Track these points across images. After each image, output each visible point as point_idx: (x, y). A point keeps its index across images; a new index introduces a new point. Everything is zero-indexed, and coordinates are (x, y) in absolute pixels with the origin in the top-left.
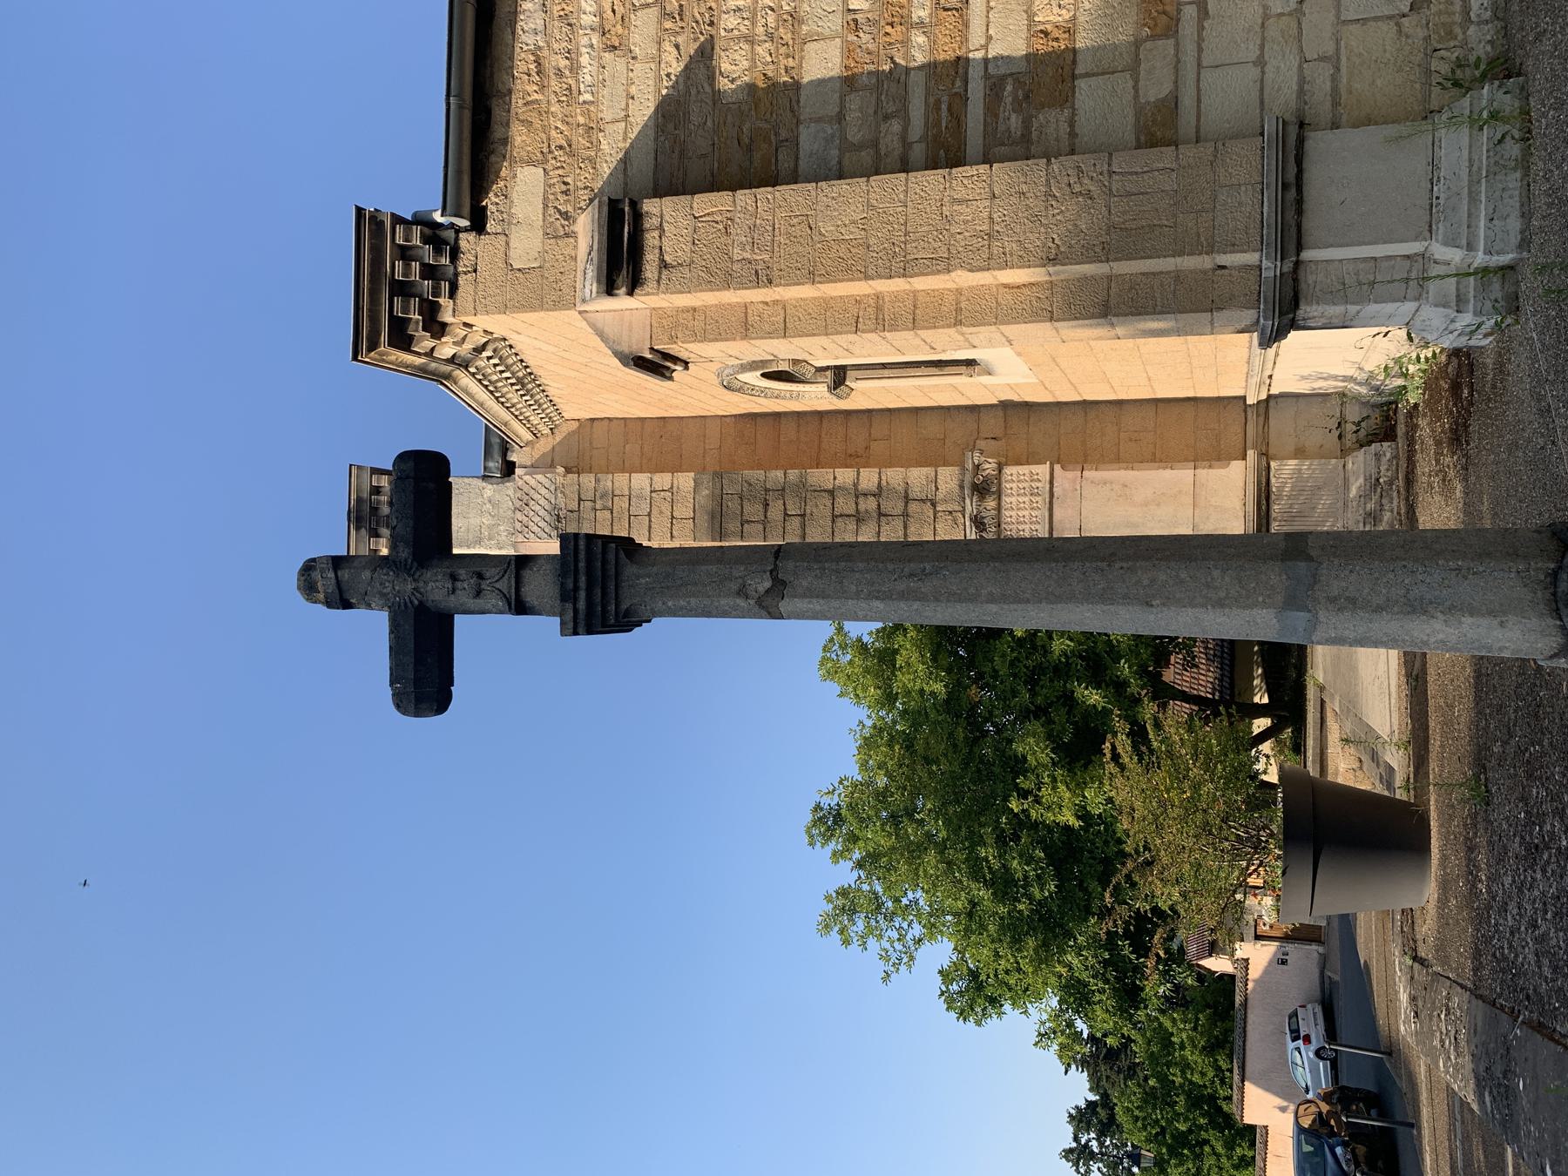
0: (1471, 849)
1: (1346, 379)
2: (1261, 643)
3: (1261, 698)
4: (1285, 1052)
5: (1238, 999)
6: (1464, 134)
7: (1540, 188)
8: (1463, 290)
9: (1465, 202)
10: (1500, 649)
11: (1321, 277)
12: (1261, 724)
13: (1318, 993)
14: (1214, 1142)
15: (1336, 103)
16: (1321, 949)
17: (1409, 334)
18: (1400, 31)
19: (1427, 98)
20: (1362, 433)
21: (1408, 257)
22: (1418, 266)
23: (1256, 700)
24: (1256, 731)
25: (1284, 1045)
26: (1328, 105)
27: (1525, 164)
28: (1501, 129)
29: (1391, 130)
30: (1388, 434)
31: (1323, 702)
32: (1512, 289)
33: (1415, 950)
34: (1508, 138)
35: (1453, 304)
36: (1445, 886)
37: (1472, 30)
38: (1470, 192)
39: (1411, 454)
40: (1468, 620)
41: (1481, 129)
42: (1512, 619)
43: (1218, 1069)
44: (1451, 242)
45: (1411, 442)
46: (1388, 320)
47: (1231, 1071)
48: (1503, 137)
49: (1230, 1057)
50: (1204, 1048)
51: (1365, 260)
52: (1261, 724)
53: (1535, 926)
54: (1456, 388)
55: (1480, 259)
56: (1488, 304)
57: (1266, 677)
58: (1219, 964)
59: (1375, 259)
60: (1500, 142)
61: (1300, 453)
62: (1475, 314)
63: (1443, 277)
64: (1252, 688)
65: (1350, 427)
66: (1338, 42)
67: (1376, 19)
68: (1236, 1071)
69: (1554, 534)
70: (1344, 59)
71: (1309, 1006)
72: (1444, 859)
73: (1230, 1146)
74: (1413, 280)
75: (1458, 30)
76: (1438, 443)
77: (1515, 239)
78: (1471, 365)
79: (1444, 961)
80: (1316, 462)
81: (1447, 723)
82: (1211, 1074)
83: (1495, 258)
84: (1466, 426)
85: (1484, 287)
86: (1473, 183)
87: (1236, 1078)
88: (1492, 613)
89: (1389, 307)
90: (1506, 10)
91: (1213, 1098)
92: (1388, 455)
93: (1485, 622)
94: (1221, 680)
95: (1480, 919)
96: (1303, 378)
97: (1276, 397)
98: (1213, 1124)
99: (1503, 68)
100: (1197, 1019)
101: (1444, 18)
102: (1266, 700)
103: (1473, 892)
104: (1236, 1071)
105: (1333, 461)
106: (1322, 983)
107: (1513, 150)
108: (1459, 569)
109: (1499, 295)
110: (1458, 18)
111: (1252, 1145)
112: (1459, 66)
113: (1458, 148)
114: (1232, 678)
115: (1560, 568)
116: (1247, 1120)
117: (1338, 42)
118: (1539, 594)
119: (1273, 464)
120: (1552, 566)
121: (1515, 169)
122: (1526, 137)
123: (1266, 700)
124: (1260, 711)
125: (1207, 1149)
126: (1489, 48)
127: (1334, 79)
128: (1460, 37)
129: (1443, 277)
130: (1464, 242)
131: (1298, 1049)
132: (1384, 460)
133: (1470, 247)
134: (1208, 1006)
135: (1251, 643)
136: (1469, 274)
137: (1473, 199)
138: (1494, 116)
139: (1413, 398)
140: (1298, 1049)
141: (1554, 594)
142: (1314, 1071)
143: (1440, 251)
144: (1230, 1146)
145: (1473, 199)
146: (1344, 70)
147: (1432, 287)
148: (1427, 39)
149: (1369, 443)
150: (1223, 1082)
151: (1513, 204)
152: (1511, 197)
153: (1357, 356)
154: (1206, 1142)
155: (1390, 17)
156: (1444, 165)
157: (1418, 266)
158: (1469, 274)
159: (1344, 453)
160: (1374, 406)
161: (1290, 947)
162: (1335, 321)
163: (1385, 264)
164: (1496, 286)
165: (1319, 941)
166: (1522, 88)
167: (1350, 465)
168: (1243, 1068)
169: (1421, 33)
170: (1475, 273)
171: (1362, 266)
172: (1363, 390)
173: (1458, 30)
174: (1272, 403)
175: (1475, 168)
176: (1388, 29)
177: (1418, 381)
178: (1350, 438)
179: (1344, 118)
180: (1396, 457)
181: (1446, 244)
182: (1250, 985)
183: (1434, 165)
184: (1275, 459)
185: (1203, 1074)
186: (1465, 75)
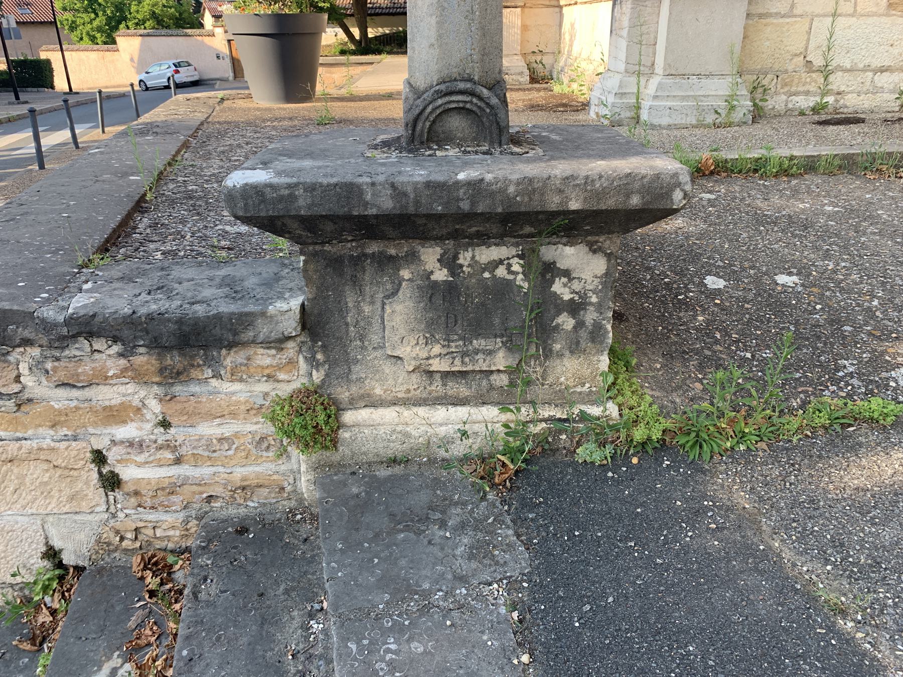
0: (290, 119)
1: (570, 52)
2: (405, 32)
3: (371, 33)
4: (166, 59)
5: (189, 31)
6: (725, 91)
7: (685, 132)
8: (628, 96)
9: (683, 94)
10: (413, 48)
11: (649, 10)
12: (356, 32)
13: (205, 77)
14: (98, 20)
15: (761, 16)
16: (231, 78)
17: (601, 73)
18: (796, 55)
19: (750, 72)
20: (535, 65)
21: (653, 65)
22: (647, 71)
23: (369, 30)
24: (352, 30)
25: (170, 59)
26: (761, 11)
27: (700, 125)
28: (723, 113)
29: (737, 49)
30: (533, 80)
31: (372, 63)
32: (625, 123)
33: (228, 99)
34: (717, 116)
35: (621, 91)
36: (269, 110)
37: (784, 97)
38: (689, 96)
39: (524, 90)
40: (433, 20)
41: (726, 101)
42: (436, 52)
43: (144, 22)
44: (660, 86)
45: (528, 90)
46: (613, 56)
47: (145, 28)
48: (719, 114)
49: (153, 28)
50: (154, 12)
51: (656, 38)
52: (356, 32)
53: (247, 144)
54: (565, 105)
55: (646, 104)
56: (618, 110)
57: (385, 35)
58: (208, 20)
59: (655, 44)
60: (716, 112)
61: (525, 28)
62: (613, 103)
63: (638, 84)
64: (377, 27)
65: (539, 58)
66: (801, 16)
67: (808, 40)
68: (145, 31)
69: (498, 82)
70: (788, 20)
71: (196, 73)
72: (285, 109)
73: (99, 29)
74: (640, 69)
75: (786, 89)
76: (530, 100)
77: (656, 121)
78: (578, 111)
79: (221, 111)
80: (519, 37)
81: (364, 108)
82: (140, 16)
83: (646, 111)
84: (541, 110)
85: (629, 107)
86: (695, 98)
87: (142, 32)
88: (440, 37)
89: (622, 56)
90: (791, 115)
91: (125, 19)
92: (522, 80)
93: (433, 33)
94: (379, 8)
95: (249, 124)
96: (572, 25)
97: (561, 12)
98: (109, 19)
99: (758, 115)
100: (170, 8)
101: (796, 81)
102: (370, 35)
103: (264, 121)
104: (145, 31)
105: (519, 48)
106: (212, 80)
107: (710, 119)
108: (473, 12)
109: (622, 116)
110: (793, 89)
111: (105, 43)
112: (765, 90)
113: (717, 89)
114: (381, 14)
115: (475, 83)
116: (118, 39)
117: (801, 16)
118: (455, 70)
119: (519, 9)
120: (476, 78)
121: (698, 120)
122: (716, 126)
123: (370, 35)
124: (364, 33)
125: (93, 16)
126: (770, 107)
127: (777, 14)
128: (782, 91)
129: (638, 84)
130: (658, 94)
131: (169, 67)
132: (519, 77)
133: (656, 97)
134: (180, 14)
135: (405, 24)
136: (638, 99)
137: (684, 98)
138: (733, 108)
139: (557, 89)
140: (169, 67)
141: (455, 80)
142: (159, 76)
143: (654, 82)
144: (99, 29)
145: (684, 98)
146: (781, 20)
147: (633, 79)
148: (786, 72)
149: (529, 69)
150: (137, 24)
151: (678, 120)
152: (682, 119)
153: (584, 55)
154: (97, 15)
155: (806, 49)
156: (708, 81)
157: (647, 71)
158: (638, 99)
159: (524, 55)
160: (551, 72)
161: (228, 61)
162: (616, 25)
163: (651, 50)
164: (628, 114)
165: (235, 77)
166: (745, 123)
167: (516, 57)
168: (148, 35)
169: (790, 68)
170: (638, 102)
171: (652, 36)
172: (562, 64)
173: (786, 89)
174: (557, 10)
175: (703, 98)
176: (799, 47)
177: (566, 90)
178: (533, 58)
179: (751, 22)
180: (520, 84)
181: (660, 84)
182: (199, 38)
183: (709, 76)
184: (522, 12)
185: (138, 12)
186: (758, 95)
